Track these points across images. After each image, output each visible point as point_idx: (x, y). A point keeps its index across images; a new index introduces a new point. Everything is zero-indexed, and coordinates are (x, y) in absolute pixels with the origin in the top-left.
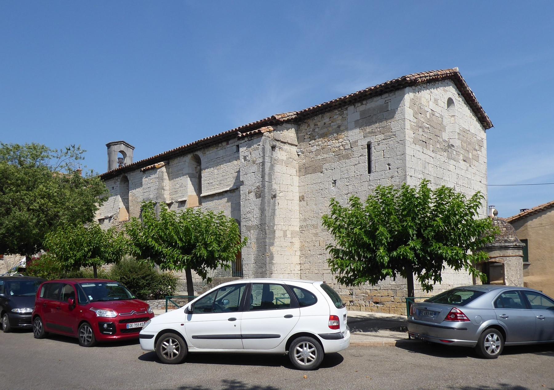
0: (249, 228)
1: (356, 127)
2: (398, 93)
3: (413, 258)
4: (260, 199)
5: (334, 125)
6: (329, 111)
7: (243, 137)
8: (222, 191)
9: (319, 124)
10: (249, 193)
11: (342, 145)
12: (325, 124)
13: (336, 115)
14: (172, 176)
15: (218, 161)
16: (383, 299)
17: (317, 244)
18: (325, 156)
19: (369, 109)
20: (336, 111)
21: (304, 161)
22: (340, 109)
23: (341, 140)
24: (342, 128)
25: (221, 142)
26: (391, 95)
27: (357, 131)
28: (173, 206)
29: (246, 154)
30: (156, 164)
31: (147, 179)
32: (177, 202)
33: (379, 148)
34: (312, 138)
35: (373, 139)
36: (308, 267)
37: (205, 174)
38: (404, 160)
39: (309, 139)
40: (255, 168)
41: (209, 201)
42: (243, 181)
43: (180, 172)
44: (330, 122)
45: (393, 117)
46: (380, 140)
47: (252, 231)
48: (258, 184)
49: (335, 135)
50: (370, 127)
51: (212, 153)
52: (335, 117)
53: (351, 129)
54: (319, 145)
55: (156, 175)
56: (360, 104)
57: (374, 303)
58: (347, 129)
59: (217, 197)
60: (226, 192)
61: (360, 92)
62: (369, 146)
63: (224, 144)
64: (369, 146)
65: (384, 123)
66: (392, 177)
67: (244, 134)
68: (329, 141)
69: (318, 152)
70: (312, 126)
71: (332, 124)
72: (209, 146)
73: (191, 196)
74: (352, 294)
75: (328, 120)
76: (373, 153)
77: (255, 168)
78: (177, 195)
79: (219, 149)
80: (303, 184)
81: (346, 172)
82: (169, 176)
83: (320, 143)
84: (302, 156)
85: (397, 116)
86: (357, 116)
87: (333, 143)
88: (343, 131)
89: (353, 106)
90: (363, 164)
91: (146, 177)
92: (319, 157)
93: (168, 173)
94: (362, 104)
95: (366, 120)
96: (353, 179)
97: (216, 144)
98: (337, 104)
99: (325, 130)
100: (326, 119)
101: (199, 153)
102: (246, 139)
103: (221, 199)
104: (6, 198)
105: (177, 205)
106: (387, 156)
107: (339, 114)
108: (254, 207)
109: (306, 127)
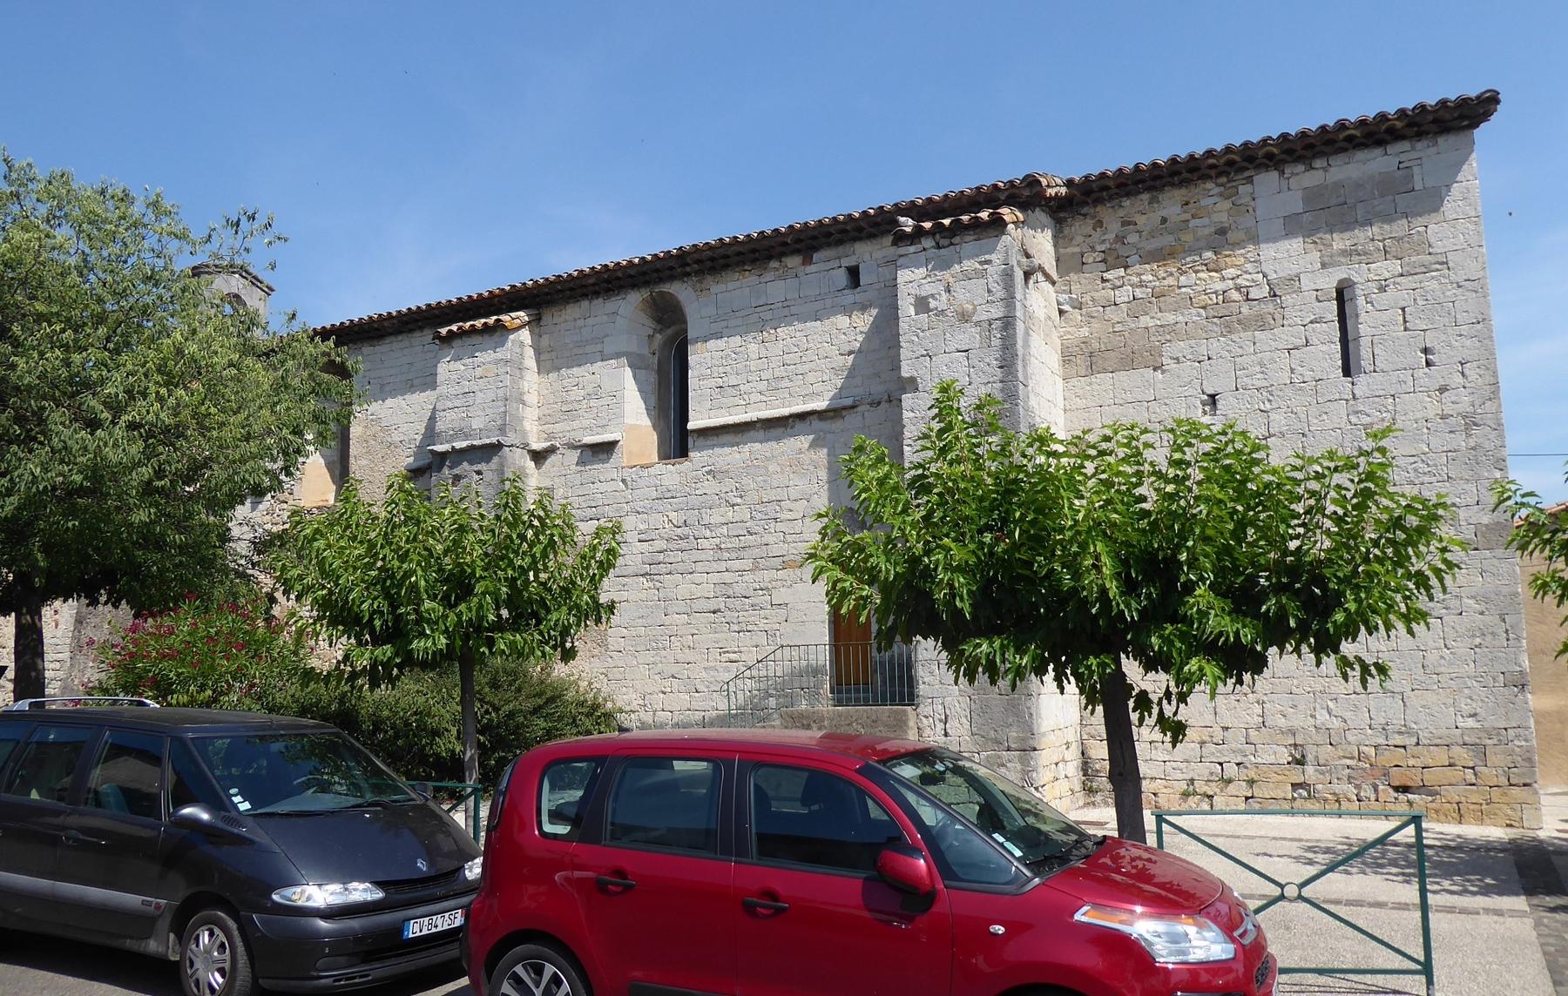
1: (1289, 234)
2: (1445, 142)
3: (1254, 641)
5: (1203, 227)
6: (1182, 183)
7: (919, 233)
8: (786, 411)
9: (1141, 220)
12: (1164, 220)
13: (1212, 201)
14: (549, 361)
16: (1430, 777)
18: (1170, 318)
19: (1339, 185)
20: (1209, 185)
21: (1085, 331)
22: (1224, 180)
23: (1231, 272)
25: (780, 256)
26: (1419, 145)
27: (1296, 244)
28: (552, 459)
29: (928, 289)
30: (504, 318)
31: (458, 365)
32: (572, 447)
33: (1383, 300)
34: (1114, 259)
35: (1361, 275)
37: (698, 357)
39: (1102, 266)
40: (969, 336)
41: (722, 446)
42: (912, 380)
43: (588, 349)
45: (1436, 210)
46: (1387, 275)
48: (983, 391)
49: (1209, 254)
50: (1347, 235)
51: (735, 288)
52: (1203, 202)
54: (1142, 285)
55: (501, 353)
56: (1301, 168)
57: (1396, 789)
58: (1255, 239)
60: (802, 416)
61: (776, 230)
62: (1342, 295)
63: (793, 261)
64: (1342, 295)
65: (1400, 227)
66: (1443, 390)
67: (927, 225)
70: (1114, 227)
71: (1193, 223)
72: (726, 267)
74: (1301, 762)
75: (1178, 209)
76: (1363, 317)
78: (575, 424)
79: (769, 276)
80: (1080, 403)
81: (1258, 369)
82: (538, 362)
84: (1076, 315)
86: (1293, 202)
87: (1201, 281)
89: (1274, 175)
90: (1324, 348)
91: (457, 358)
92: (1145, 321)
93: (538, 353)
95: (1325, 216)
96: (1289, 391)
97: (753, 261)
98: (632, 272)
99: (1167, 240)
100: (1171, 204)
101: (680, 291)
102: (928, 243)
103: (778, 439)
104: (25, 369)
106: (1415, 322)
107: (1221, 195)
109: (1089, 230)
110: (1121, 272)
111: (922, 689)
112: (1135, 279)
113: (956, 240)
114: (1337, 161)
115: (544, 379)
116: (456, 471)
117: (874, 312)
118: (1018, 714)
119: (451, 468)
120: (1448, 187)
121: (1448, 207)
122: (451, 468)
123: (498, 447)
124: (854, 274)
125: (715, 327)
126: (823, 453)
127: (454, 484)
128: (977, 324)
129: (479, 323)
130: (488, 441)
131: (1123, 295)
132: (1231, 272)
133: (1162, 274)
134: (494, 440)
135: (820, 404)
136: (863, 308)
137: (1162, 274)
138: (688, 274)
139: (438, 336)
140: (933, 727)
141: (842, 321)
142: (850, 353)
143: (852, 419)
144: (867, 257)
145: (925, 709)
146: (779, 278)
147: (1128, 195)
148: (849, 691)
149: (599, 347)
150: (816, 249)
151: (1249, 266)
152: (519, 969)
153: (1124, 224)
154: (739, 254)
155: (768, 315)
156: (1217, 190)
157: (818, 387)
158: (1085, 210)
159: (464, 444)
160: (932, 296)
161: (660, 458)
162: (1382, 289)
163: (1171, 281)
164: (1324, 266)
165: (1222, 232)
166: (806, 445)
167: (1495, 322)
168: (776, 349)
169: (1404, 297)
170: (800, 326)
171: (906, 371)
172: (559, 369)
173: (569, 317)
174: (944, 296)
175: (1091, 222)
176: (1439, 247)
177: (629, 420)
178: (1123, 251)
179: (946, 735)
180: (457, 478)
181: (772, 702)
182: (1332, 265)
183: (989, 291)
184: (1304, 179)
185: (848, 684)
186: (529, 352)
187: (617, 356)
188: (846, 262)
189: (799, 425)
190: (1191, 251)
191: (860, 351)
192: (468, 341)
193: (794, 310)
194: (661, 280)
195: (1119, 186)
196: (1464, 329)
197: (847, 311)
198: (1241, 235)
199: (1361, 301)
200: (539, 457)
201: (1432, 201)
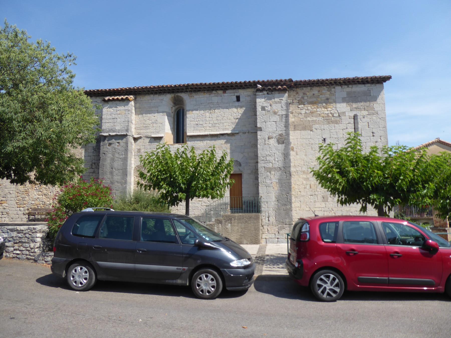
0: (269, 170)
4: (283, 145)
5: (323, 97)
6: (319, 86)
8: (218, 133)
9: (308, 94)
10: (269, 138)
11: (331, 113)
12: (314, 94)
13: (324, 90)
15: (212, 106)
17: (308, 187)
18: (315, 119)
19: (355, 92)
20: (325, 87)
22: (328, 87)
23: (330, 109)
24: (330, 100)
25: (216, 90)
27: (344, 105)
29: (265, 105)
31: (111, 110)
32: (147, 137)
33: (364, 120)
35: (360, 114)
36: (299, 205)
38: (385, 131)
39: (298, 104)
40: (276, 118)
41: (198, 141)
43: (153, 109)
44: (319, 94)
47: (273, 173)
49: (324, 104)
50: (356, 104)
53: (340, 103)
54: (308, 110)
55: (126, 108)
56: (346, 87)
58: (335, 102)
59: (210, 138)
60: (222, 135)
63: (220, 92)
64: (355, 117)
68: (318, 108)
69: (306, 115)
70: (301, 94)
72: (199, 91)
73: (167, 133)
76: (359, 123)
77: (276, 118)
78: (148, 131)
79: (212, 95)
83: (309, 108)
85: (379, 100)
86: (344, 94)
87: (322, 110)
88: (331, 103)
89: (340, 87)
91: (110, 107)
92: (309, 119)
93: (135, 109)
94: (348, 87)
95: (351, 99)
97: (208, 90)
98: (170, 89)
99: (314, 99)
100: (315, 91)
101: (185, 96)
103: (215, 140)
105: (148, 140)
106: (370, 126)
107: (327, 90)
108: (274, 150)
110: (303, 106)
111: (262, 209)
112: (306, 108)
113: (273, 93)
114: (354, 86)
115: (137, 117)
116: (110, 142)
117: (244, 108)
118: (289, 216)
119: (108, 141)
120: (378, 96)
121: (378, 100)
122: (108, 141)
123: (126, 135)
124: (238, 99)
125: (195, 107)
126: (229, 145)
127: (109, 146)
128: (279, 115)
129: (120, 98)
130: (123, 134)
131: (303, 112)
132: (330, 109)
133: (313, 107)
134: (125, 133)
135: (229, 132)
136: (241, 107)
137: (313, 107)
138: (187, 91)
139: (104, 100)
140: (265, 219)
141: (235, 110)
142: (237, 119)
143: (237, 137)
144: (242, 94)
145: (263, 214)
146: (216, 96)
147: (305, 87)
148: (237, 209)
149: (157, 109)
150: (227, 89)
151: (334, 108)
152: (322, 277)
153: (304, 94)
154: (205, 88)
155: (212, 106)
156: (326, 89)
157: (227, 127)
158: (294, 89)
159: (114, 134)
160: (266, 107)
161: (174, 143)
162: (364, 117)
163: (315, 110)
164: (351, 110)
165: (328, 99)
166: (224, 143)
167: (388, 128)
168: (214, 115)
169: (368, 120)
170: (222, 110)
171: (259, 125)
172: (142, 114)
173: (147, 98)
174: (270, 107)
175: (295, 92)
176: (376, 109)
177: (166, 131)
178: (303, 101)
179: (269, 221)
180: (110, 144)
181: (212, 212)
182: (353, 110)
183: (282, 107)
184: (347, 89)
185: (237, 207)
186: (134, 108)
187: (163, 112)
188: (238, 94)
189: (221, 137)
190: (320, 103)
191: (240, 118)
192: (114, 102)
193: (220, 105)
194: (178, 92)
195: (304, 84)
196: (381, 129)
197: (236, 107)
198: (332, 101)
199: (359, 120)
200: (135, 139)
201: (375, 99)
